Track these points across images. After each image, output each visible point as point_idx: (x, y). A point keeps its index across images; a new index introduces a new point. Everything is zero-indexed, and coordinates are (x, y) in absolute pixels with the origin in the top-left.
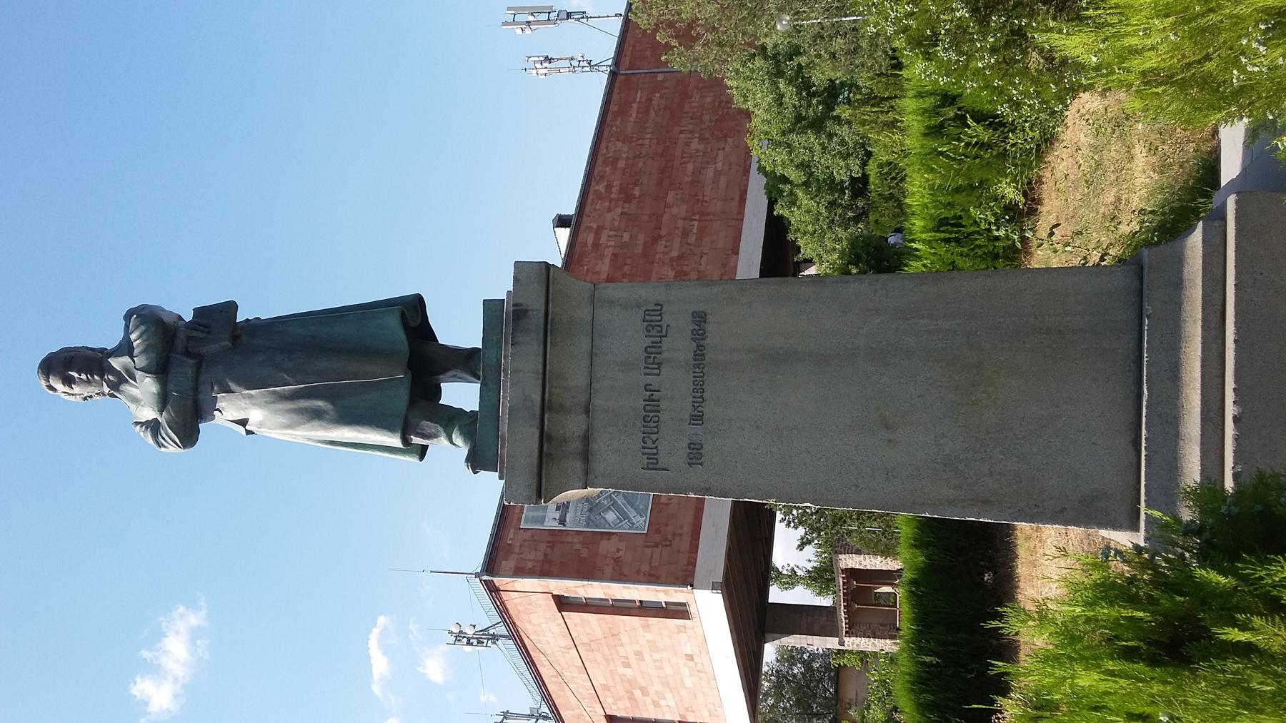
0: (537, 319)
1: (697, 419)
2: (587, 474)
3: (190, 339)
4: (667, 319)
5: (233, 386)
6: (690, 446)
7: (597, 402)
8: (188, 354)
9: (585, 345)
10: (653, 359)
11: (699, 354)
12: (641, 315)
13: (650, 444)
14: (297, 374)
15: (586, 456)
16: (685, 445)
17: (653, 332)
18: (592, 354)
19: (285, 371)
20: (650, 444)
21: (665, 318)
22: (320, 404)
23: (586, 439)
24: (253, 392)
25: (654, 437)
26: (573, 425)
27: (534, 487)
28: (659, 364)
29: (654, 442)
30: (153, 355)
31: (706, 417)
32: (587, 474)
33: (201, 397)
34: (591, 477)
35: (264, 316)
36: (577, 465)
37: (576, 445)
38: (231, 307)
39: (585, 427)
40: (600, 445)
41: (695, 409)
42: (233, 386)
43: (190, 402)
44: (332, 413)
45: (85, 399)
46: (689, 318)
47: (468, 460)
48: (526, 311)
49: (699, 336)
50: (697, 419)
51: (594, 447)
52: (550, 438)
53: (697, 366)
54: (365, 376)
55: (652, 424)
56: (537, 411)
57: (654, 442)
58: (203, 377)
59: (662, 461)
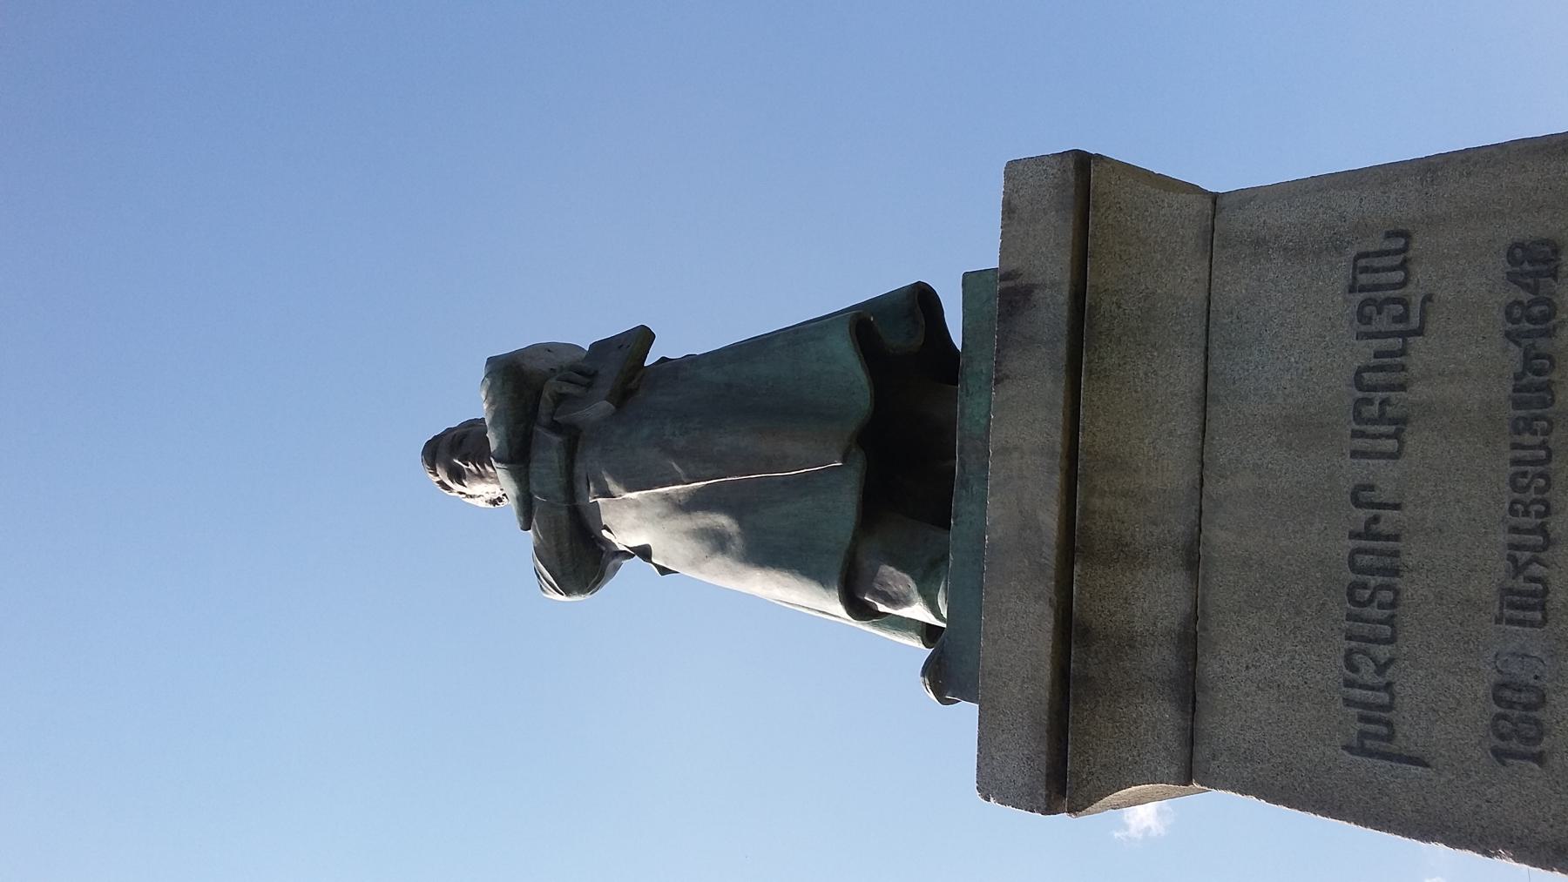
0: (1052, 309)
1: (1526, 602)
2: (1190, 740)
3: (560, 398)
4: (1423, 277)
5: (614, 487)
6: (1502, 691)
7: (1218, 536)
8: (555, 427)
9: (1184, 374)
10: (1379, 407)
11: (1533, 388)
12: (1342, 271)
13: (1367, 673)
14: (696, 462)
15: (1188, 692)
16: (1483, 690)
17: (1382, 323)
18: (1204, 399)
19: (677, 455)
20: (1367, 673)
21: (1420, 273)
22: (723, 521)
23: (1190, 640)
24: (634, 495)
25: (1383, 652)
26: (1151, 600)
27: (1042, 762)
28: (1401, 422)
29: (1381, 668)
30: (502, 429)
31: (1557, 599)
32: (1190, 740)
33: (580, 502)
34: (1202, 752)
35: (699, 351)
36: (1162, 715)
37: (1160, 658)
38: (644, 336)
39: (1184, 606)
40: (1222, 664)
41: (1518, 568)
42: (614, 487)
43: (564, 513)
44: (738, 540)
45: (494, 502)
46: (1499, 266)
47: (926, 671)
48: (1028, 291)
49: (1531, 323)
50: (1526, 602)
51: (1210, 667)
52: (1086, 631)
53: (1528, 425)
54: (782, 463)
55: (1374, 612)
56: (1050, 555)
57: (1381, 668)
58: (580, 469)
59: (1409, 736)
